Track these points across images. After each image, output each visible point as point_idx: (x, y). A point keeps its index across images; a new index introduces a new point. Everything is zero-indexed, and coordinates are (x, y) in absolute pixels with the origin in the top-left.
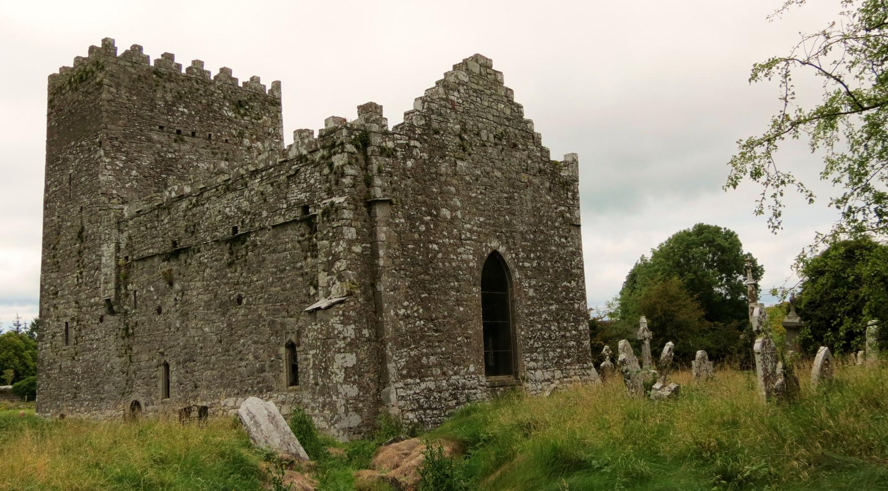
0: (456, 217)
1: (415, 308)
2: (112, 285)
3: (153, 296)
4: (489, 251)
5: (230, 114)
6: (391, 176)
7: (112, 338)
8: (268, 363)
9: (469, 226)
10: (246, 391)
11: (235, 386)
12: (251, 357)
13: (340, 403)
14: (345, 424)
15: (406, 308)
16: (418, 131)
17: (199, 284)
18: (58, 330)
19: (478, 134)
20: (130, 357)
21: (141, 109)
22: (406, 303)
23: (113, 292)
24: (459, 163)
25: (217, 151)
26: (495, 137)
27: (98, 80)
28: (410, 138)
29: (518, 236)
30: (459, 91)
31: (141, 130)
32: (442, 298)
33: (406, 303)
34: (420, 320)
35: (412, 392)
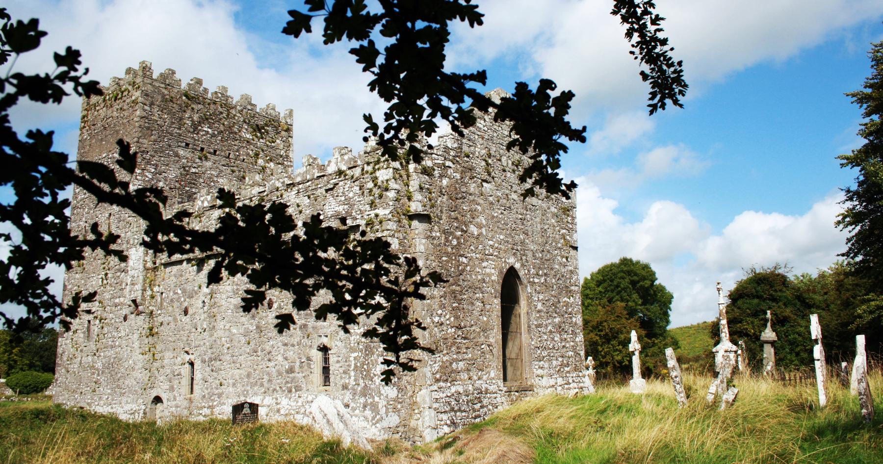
0: (481, 233)
1: (448, 317)
2: (139, 287)
3: (179, 298)
4: (508, 267)
5: (248, 136)
6: (430, 193)
7: (136, 336)
8: (298, 364)
9: (491, 243)
10: (275, 390)
11: (262, 385)
12: (280, 358)
13: (382, 403)
14: (385, 424)
15: (440, 316)
16: (452, 153)
17: (229, 288)
18: (80, 327)
19: (500, 160)
20: (154, 355)
21: (170, 127)
22: (440, 312)
23: (139, 293)
24: (485, 184)
25: (235, 168)
26: (513, 164)
27: (133, 98)
28: (445, 159)
29: (530, 254)
30: (485, 121)
31: (170, 146)
32: (470, 307)
33: (440, 312)
34: (452, 327)
35: (445, 395)
